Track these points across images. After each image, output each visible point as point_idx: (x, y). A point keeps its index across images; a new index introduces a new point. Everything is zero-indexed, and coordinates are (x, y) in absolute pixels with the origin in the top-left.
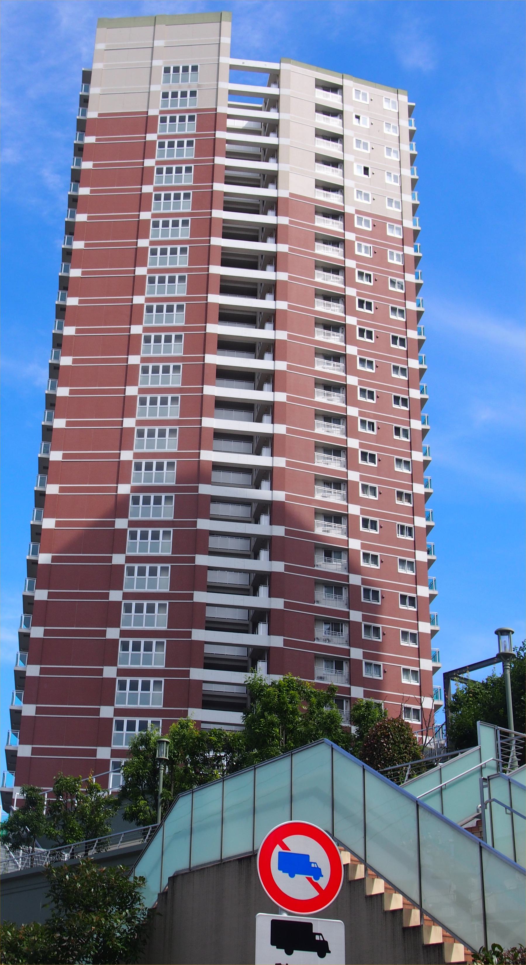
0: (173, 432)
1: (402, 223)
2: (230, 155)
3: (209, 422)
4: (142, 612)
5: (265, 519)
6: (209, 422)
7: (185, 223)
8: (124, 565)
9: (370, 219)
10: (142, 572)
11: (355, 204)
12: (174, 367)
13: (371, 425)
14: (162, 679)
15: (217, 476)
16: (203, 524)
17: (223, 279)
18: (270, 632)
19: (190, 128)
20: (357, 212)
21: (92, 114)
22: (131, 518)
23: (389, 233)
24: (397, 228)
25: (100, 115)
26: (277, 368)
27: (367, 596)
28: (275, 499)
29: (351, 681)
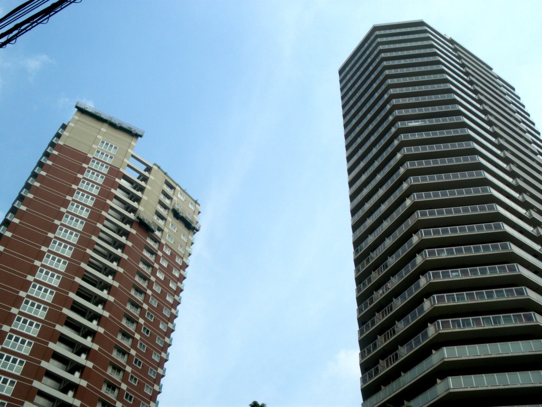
0: (37, 326)
1: (182, 258)
2: (95, 251)
3: (58, 328)
4: (26, 324)
5: (77, 374)
6: (58, 328)
7: (21, 363)
8: (7, 333)
9: (146, 346)
10: (17, 340)
11: (166, 240)
12: (20, 361)
13: (148, 331)
14: (48, 307)
15: (110, 211)
16: (99, 225)
17: (75, 302)
18: (74, 397)
19: (105, 170)
20: (166, 244)
21: (61, 142)
22: (28, 293)
23: (171, 285)
24: (158, 356)
25: (64, 145)
26: (93, 347)
27: (136, 362)
28: (81, 384)
29: (140, 316)
